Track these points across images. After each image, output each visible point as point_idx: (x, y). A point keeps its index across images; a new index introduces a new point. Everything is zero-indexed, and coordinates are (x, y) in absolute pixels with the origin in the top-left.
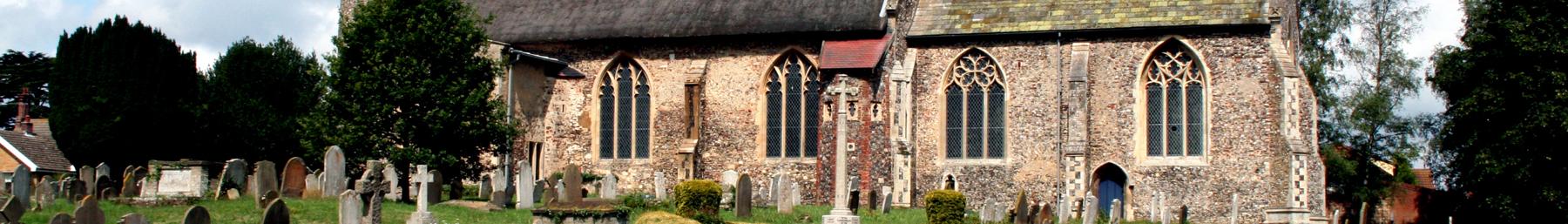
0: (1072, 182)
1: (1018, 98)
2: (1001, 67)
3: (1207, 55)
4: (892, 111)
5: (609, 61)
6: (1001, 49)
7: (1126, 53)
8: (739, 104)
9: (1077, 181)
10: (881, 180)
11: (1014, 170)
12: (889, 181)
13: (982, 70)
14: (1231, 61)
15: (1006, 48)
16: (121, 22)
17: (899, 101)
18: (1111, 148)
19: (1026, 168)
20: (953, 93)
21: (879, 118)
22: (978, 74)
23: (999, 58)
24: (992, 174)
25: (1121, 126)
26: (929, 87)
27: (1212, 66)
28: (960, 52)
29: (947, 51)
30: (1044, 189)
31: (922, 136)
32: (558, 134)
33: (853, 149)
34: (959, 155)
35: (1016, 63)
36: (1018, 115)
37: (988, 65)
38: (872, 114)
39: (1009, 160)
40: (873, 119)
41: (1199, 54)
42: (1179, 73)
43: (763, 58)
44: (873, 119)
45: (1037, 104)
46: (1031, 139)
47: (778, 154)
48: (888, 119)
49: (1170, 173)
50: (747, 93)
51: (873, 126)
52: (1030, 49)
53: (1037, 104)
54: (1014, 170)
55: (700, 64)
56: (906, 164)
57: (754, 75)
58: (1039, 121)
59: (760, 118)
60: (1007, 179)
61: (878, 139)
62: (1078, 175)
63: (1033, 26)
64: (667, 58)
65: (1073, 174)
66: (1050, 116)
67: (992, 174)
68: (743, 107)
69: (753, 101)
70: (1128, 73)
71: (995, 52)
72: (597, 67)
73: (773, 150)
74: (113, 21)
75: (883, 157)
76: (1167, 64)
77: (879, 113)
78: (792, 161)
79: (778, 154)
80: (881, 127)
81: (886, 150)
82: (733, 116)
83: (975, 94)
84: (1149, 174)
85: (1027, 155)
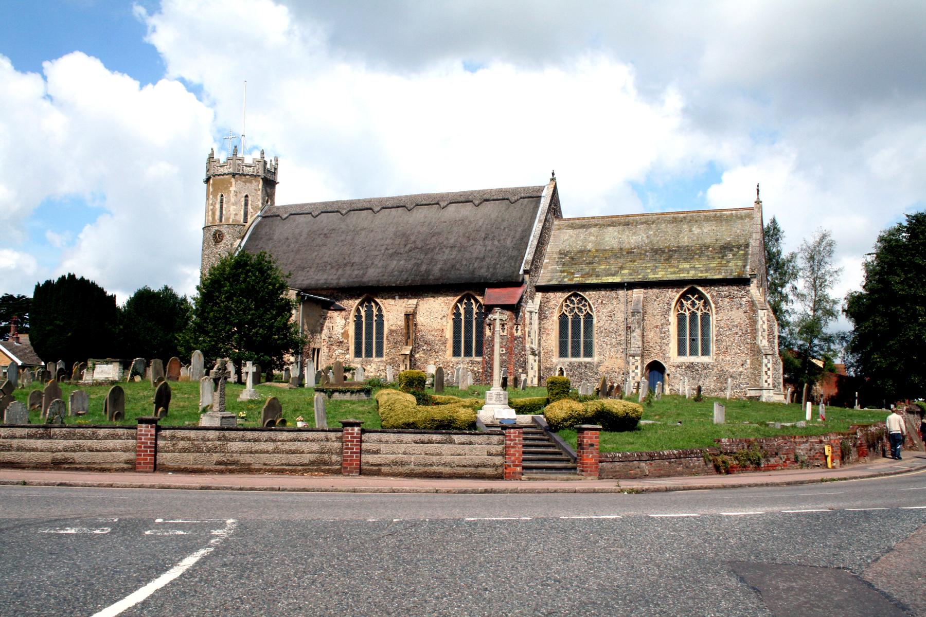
0: (633, 371)
1: (601, 322)
2: (591, 304)
3: (713, 296)
4: (527, 329)
5: (360, 300)
6: (591, 293)
7: (665, 296)
8: (436, 325)
9: (636, 371)
10: (520, 370)
11: (599, 364)
12: (525, 371)
13: (580, 305)
14: (727, 300)
15: (594, 293)
16: (72, 277)
17: (531, 324)
18: (656, 351)
19: (606, 364)
20: (563, 319)
21: (519, 333)
22: (578, 308)
23: (590, 298)
24: (586, 367)
25: (662, 338)
26: (549, 315)
27: (716, 303)
28: (567, 295)
29: (559, 294)
30: (616, 376)
31: (545, 344)
32: (329, 343)
33: (504, 352)
34: (566, 356)
35: (600, 301)
36: (601, 332)
37: (583, 302)
38: (515, 331)
39: (596, 359)
40: (515, 334)
41: (708, 296)
42: (696, 307)
43: (450, 298)
44: (515, 334)
45: (612, 325)
46: (609, 347)
47: (460, 355)
48: (524, 335)
49: (691, 366)
50: (441, 319)
51: (516, 338)
52: (608, 293)
53: (612, 325)
54: (599, 364)
55: (413, 302)
56: (535, 361)
57: (445, 308)
58: (614, 336)
59: (449, 334)
60: (595, 370)
61: (519, 346)
62: (636, 368)
63: (610, 280)
64: (394, 298)
65: (634, 367)
66: (620, 333)
67: (586, 367)
68: (439, 327)
69: (445, 324)
70: (666, 307)
71: (591, 296)
72: (352, 304)
73: (456, 353)
74: (67, 276)
75: (522, 357)
76: (689, 302)
77: (519, 331)
78: (468, 359)
79: (460, 355)
80: (521, 339)
81: (523, 353)
82: (433, 333)
83: (576, 319)
84: (678, 367)
85: (606, 355)
